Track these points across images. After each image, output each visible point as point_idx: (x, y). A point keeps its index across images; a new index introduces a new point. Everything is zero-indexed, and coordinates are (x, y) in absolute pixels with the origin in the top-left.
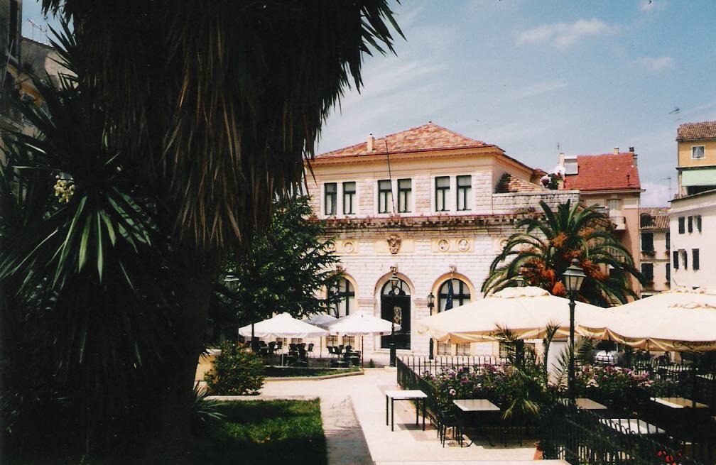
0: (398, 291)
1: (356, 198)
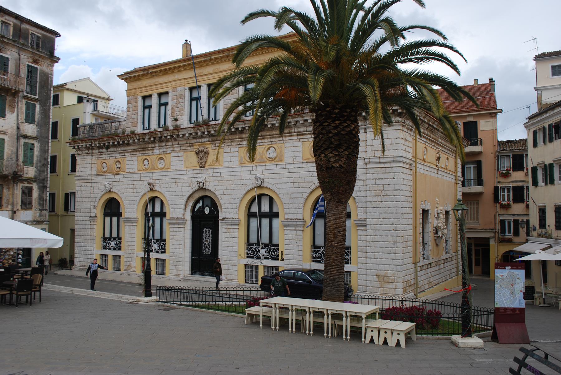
0: (208, 210)
1: (169, 107)
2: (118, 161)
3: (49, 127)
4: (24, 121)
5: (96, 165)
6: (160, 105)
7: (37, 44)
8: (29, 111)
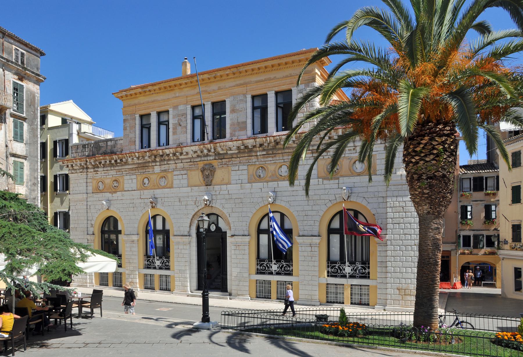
0: (215, 227)
2: (116, 180)
3: (37, 148)
4: (13, 139)
5: (91, 184)
6: (160, 123)
7: (21, 61)
8: (17, 129)
